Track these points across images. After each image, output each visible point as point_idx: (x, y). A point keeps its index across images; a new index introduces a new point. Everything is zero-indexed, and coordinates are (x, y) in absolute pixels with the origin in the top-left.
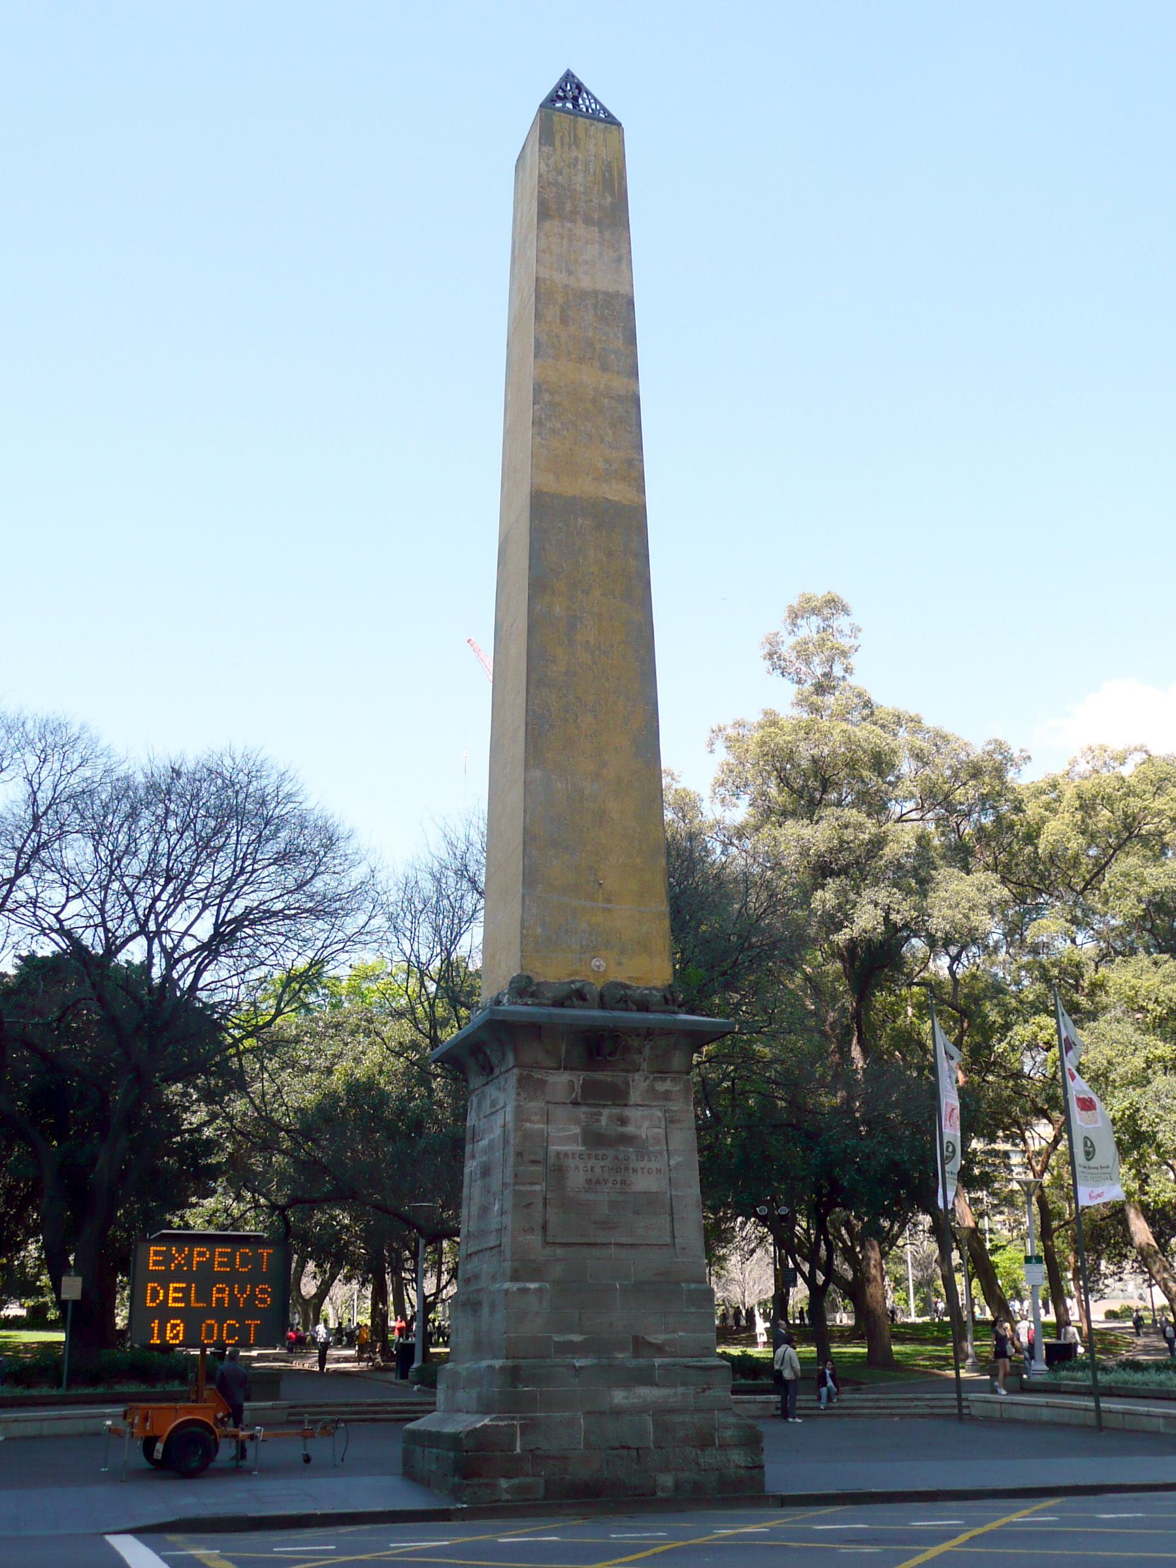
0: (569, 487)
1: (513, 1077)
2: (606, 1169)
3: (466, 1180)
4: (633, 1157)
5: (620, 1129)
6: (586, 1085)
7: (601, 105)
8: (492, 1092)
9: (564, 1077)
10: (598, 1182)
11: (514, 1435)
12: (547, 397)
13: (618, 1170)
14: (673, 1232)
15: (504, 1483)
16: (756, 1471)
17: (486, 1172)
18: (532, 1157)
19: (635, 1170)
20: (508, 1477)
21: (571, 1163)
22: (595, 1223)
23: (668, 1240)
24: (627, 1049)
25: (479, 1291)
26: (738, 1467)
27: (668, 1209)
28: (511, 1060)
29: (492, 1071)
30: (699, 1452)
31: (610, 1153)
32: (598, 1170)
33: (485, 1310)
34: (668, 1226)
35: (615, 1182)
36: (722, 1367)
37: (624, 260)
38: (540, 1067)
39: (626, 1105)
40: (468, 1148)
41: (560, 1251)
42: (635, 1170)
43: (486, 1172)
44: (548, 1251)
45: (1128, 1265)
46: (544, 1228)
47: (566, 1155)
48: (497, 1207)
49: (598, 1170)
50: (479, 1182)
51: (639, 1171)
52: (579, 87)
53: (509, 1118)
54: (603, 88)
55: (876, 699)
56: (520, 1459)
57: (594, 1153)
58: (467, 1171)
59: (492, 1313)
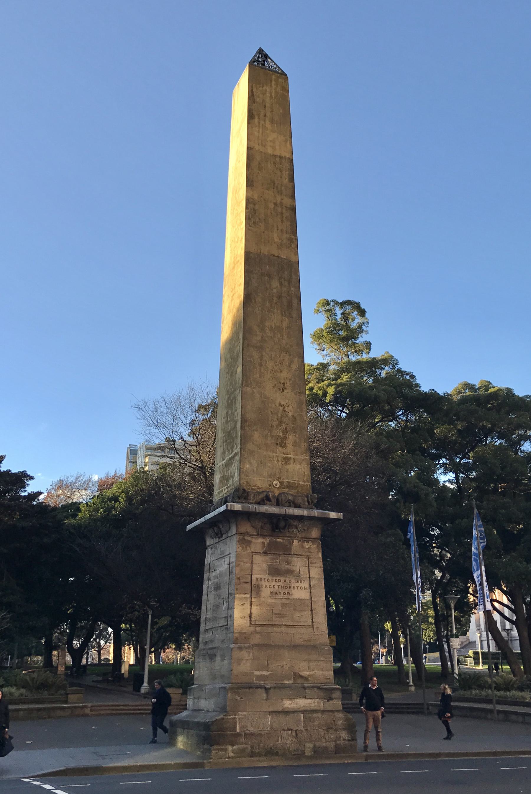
0: (265, 250)
1: (235, 539)
2: (280, 587)
3: (205, 592)
4: (293, 581)
5: (288, 566)
6: (269, 544)
7: (277, 65)
8: (221, 547)
9: (260, 540)
10: (276, 593)
11: (236, 723)
12: (251, 206)
13: (286, 587)
14: (312, 620)
15: (230, 748)
16: (352, 743)
17: (217, 587)
18: (245, 580)
19: (294, 588)
20: (233, 745)
21: (263, 583)
22: (275, 614)
23: (310, 624)
24: (290, 526)
25: (214, 648)
26: (344, 740)
27: (310, 608)
28: (234, 530)
29: (222, 536)
30: (326, 732)
31: (283, 579)
32: (276, 587)
33: (218, 658)
34: (310, 617)
35: (284, 594)
36: (337, 689)
37: (288, 142)
38: (248, 534)
39: (290, 554)
40: (206, 576)
41: (258, 629)
42: (294, 588)
43: (217, 587)
44: (252, 628)
45: (442, 708)
46: (251, 617)
47: (261, 579)
48: (225, 605)
49: (276, 587)
50: (213, 592)
51: (296, 588)
52: (266, 56)
53: (233, 559)
54: (267, 51)
55: (471, 382)
56: (239, 735)
57: (274, 578)
58: (205, 587)
59: (222, 660)
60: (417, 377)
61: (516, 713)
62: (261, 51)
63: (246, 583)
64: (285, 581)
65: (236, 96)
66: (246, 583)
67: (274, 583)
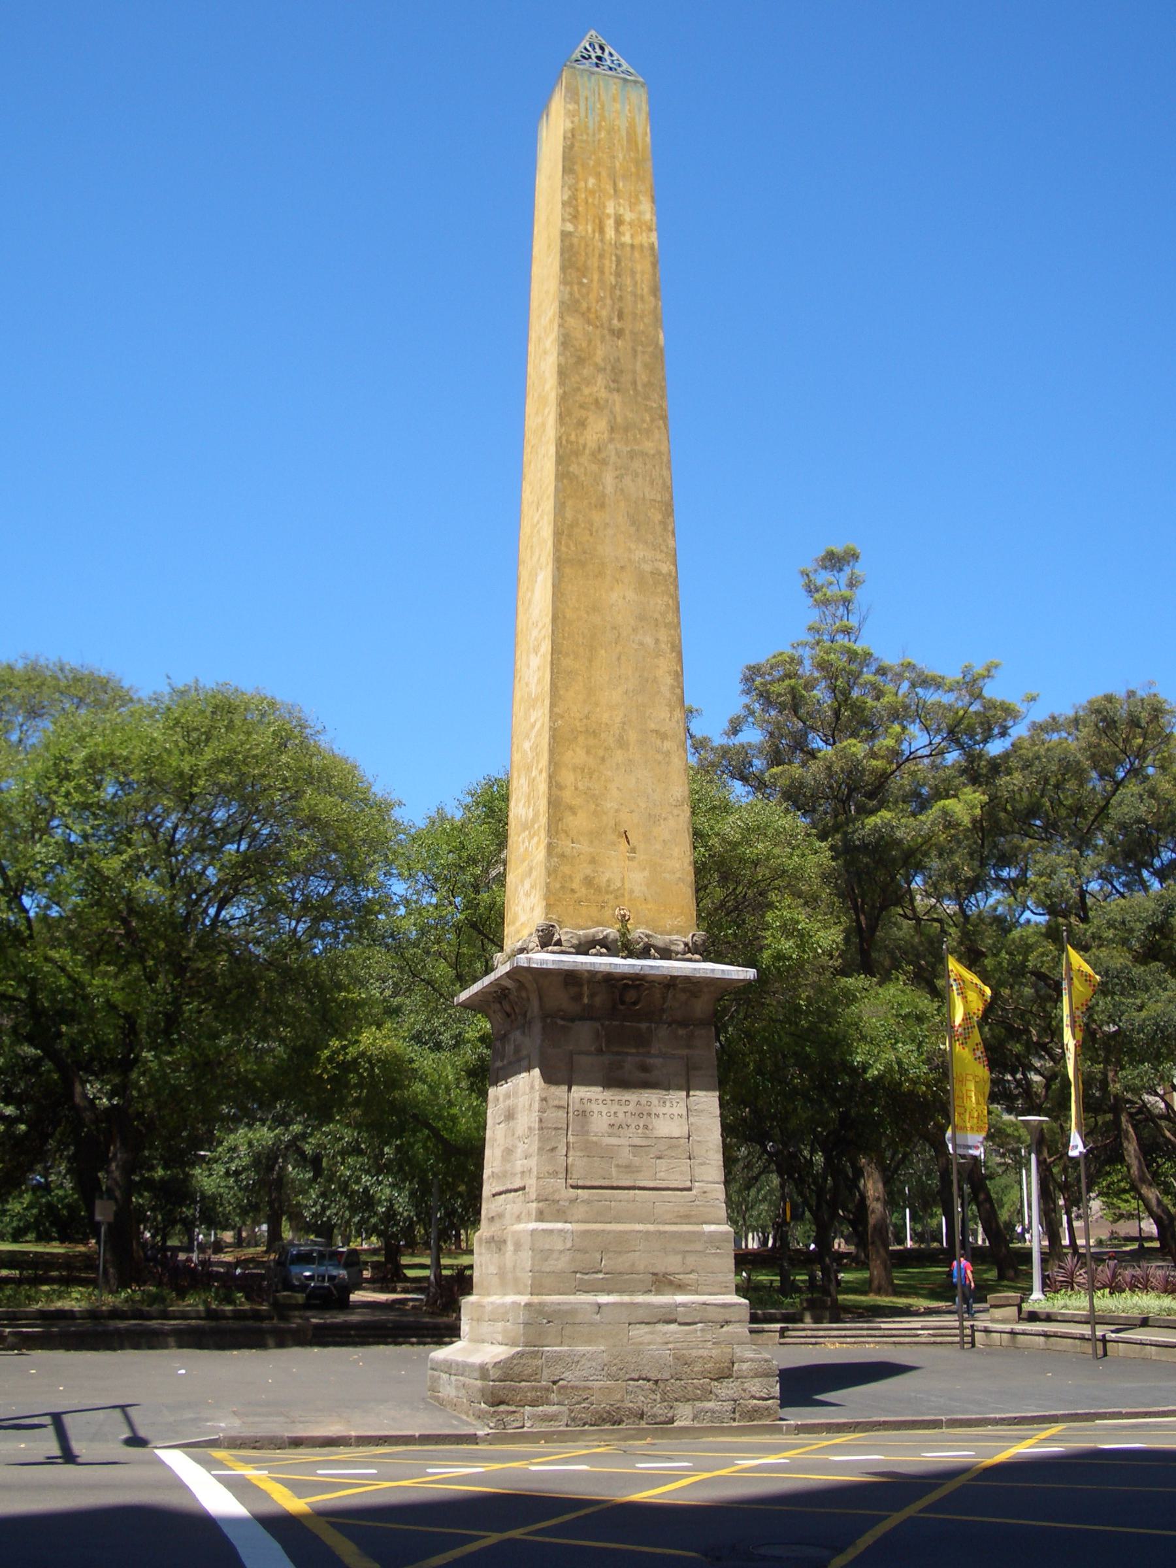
2: (629, 1114)
10: (620, 1126)
13: (641, 1115)
18: (556, 1103)
19: (657, 1116)
21: (594, 1107)
42: (657, 1116)
47: (590, 1100)
60: (1109, 690)
61: (1021, 1189)
62: (802, 573)
63: (559, 1107)
64: (638, 1103)
65: (544, 134)
66: (559, 1107)
67: (615, 1108)
